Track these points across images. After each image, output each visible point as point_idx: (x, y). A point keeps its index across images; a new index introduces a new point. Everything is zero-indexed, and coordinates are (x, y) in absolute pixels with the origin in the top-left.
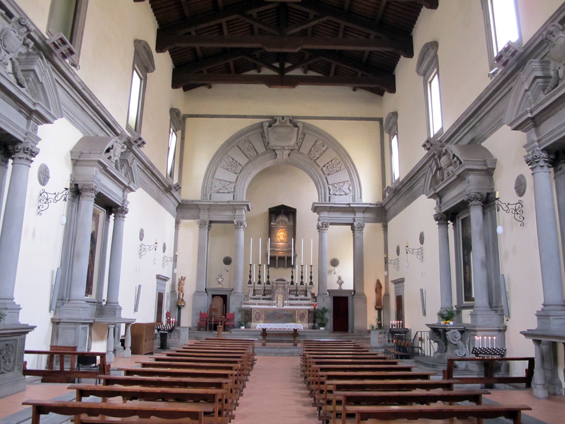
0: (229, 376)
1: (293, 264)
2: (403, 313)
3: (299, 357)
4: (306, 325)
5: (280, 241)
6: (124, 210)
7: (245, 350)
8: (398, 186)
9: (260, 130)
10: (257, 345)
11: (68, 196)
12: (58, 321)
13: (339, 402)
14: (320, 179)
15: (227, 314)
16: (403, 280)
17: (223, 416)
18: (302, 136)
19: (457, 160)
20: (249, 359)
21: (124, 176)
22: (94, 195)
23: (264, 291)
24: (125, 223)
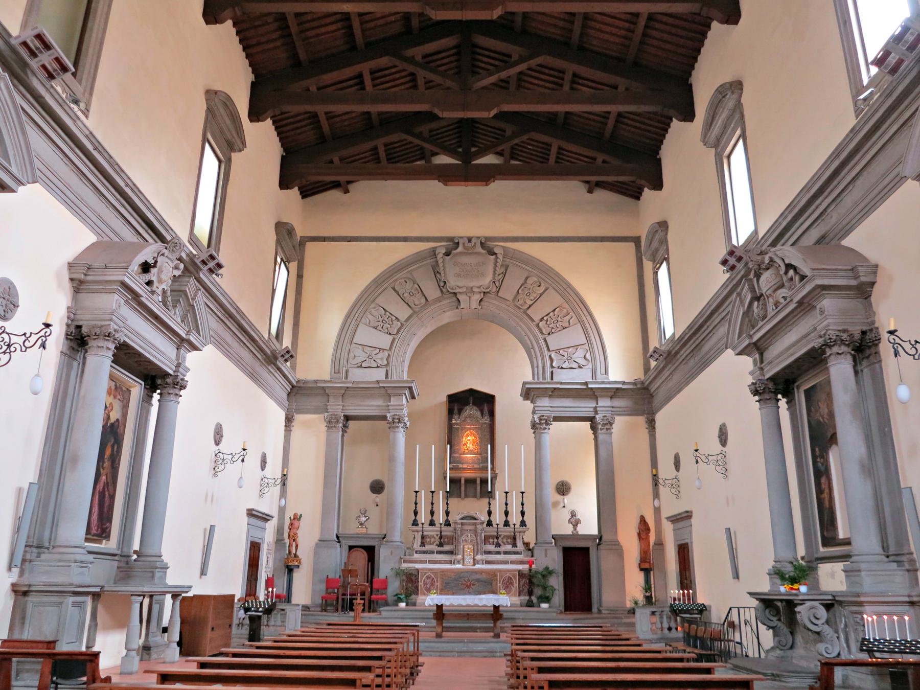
1: (490, 490)
3: (504, 660)
4: (516, 600)
12: (26, 589)
16: (689, 514)
19: (795, 275)
21: (179, 320)
22: (112, 346)
23: (441, 537)
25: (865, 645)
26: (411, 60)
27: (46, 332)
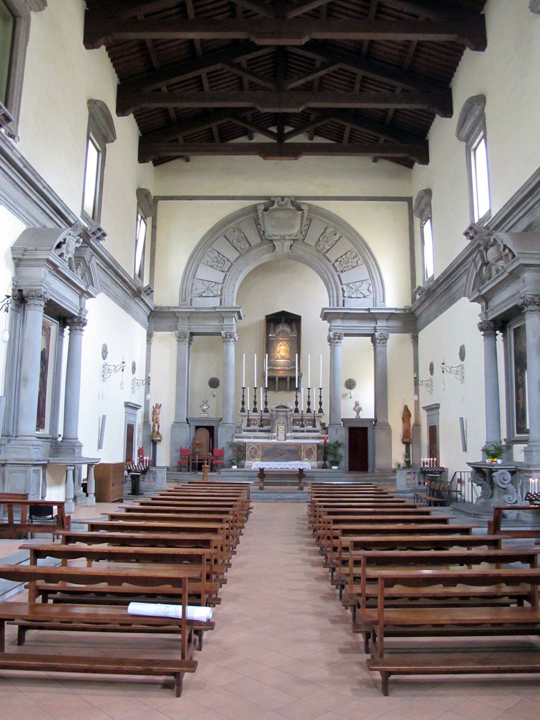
0: (218, 531)
1: (297, 387)
2: (438, 447)
4: (315, 464)
5: (280, 357)
6: (82, 322)
7: (238, 496)
8: (432, 286)
9: (253, 215)
10: (253, 488)
11: (10, 305)
12: (4, 462)
13: (357, 563)
14: (331, 278)
15: (214, 450)
17: (212, 582)
18: (308, 222)
20: (243, 508)
21: (80, 278)
23: (261, 421)
24: (83, 337)
25: (528, 497)
26: (238, 66)
27: (8, 301)
